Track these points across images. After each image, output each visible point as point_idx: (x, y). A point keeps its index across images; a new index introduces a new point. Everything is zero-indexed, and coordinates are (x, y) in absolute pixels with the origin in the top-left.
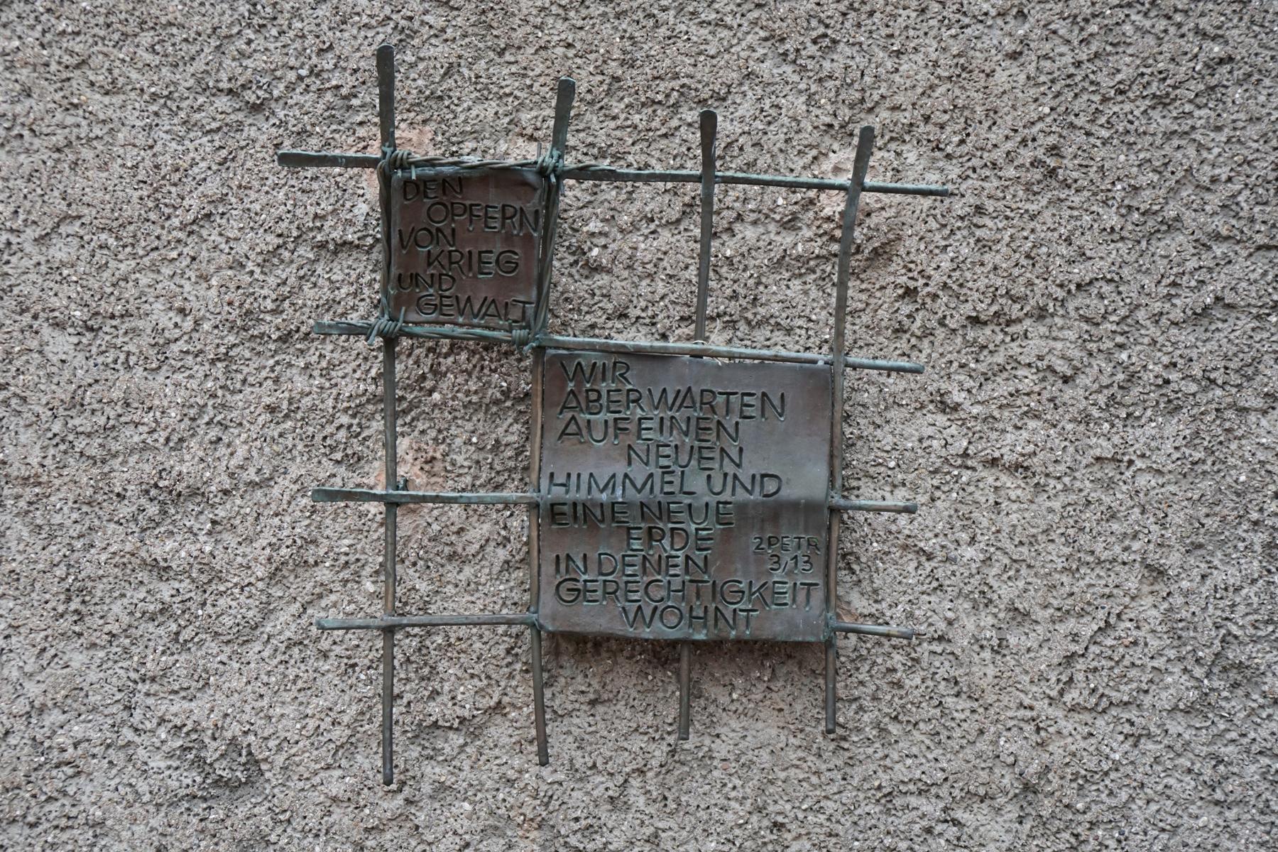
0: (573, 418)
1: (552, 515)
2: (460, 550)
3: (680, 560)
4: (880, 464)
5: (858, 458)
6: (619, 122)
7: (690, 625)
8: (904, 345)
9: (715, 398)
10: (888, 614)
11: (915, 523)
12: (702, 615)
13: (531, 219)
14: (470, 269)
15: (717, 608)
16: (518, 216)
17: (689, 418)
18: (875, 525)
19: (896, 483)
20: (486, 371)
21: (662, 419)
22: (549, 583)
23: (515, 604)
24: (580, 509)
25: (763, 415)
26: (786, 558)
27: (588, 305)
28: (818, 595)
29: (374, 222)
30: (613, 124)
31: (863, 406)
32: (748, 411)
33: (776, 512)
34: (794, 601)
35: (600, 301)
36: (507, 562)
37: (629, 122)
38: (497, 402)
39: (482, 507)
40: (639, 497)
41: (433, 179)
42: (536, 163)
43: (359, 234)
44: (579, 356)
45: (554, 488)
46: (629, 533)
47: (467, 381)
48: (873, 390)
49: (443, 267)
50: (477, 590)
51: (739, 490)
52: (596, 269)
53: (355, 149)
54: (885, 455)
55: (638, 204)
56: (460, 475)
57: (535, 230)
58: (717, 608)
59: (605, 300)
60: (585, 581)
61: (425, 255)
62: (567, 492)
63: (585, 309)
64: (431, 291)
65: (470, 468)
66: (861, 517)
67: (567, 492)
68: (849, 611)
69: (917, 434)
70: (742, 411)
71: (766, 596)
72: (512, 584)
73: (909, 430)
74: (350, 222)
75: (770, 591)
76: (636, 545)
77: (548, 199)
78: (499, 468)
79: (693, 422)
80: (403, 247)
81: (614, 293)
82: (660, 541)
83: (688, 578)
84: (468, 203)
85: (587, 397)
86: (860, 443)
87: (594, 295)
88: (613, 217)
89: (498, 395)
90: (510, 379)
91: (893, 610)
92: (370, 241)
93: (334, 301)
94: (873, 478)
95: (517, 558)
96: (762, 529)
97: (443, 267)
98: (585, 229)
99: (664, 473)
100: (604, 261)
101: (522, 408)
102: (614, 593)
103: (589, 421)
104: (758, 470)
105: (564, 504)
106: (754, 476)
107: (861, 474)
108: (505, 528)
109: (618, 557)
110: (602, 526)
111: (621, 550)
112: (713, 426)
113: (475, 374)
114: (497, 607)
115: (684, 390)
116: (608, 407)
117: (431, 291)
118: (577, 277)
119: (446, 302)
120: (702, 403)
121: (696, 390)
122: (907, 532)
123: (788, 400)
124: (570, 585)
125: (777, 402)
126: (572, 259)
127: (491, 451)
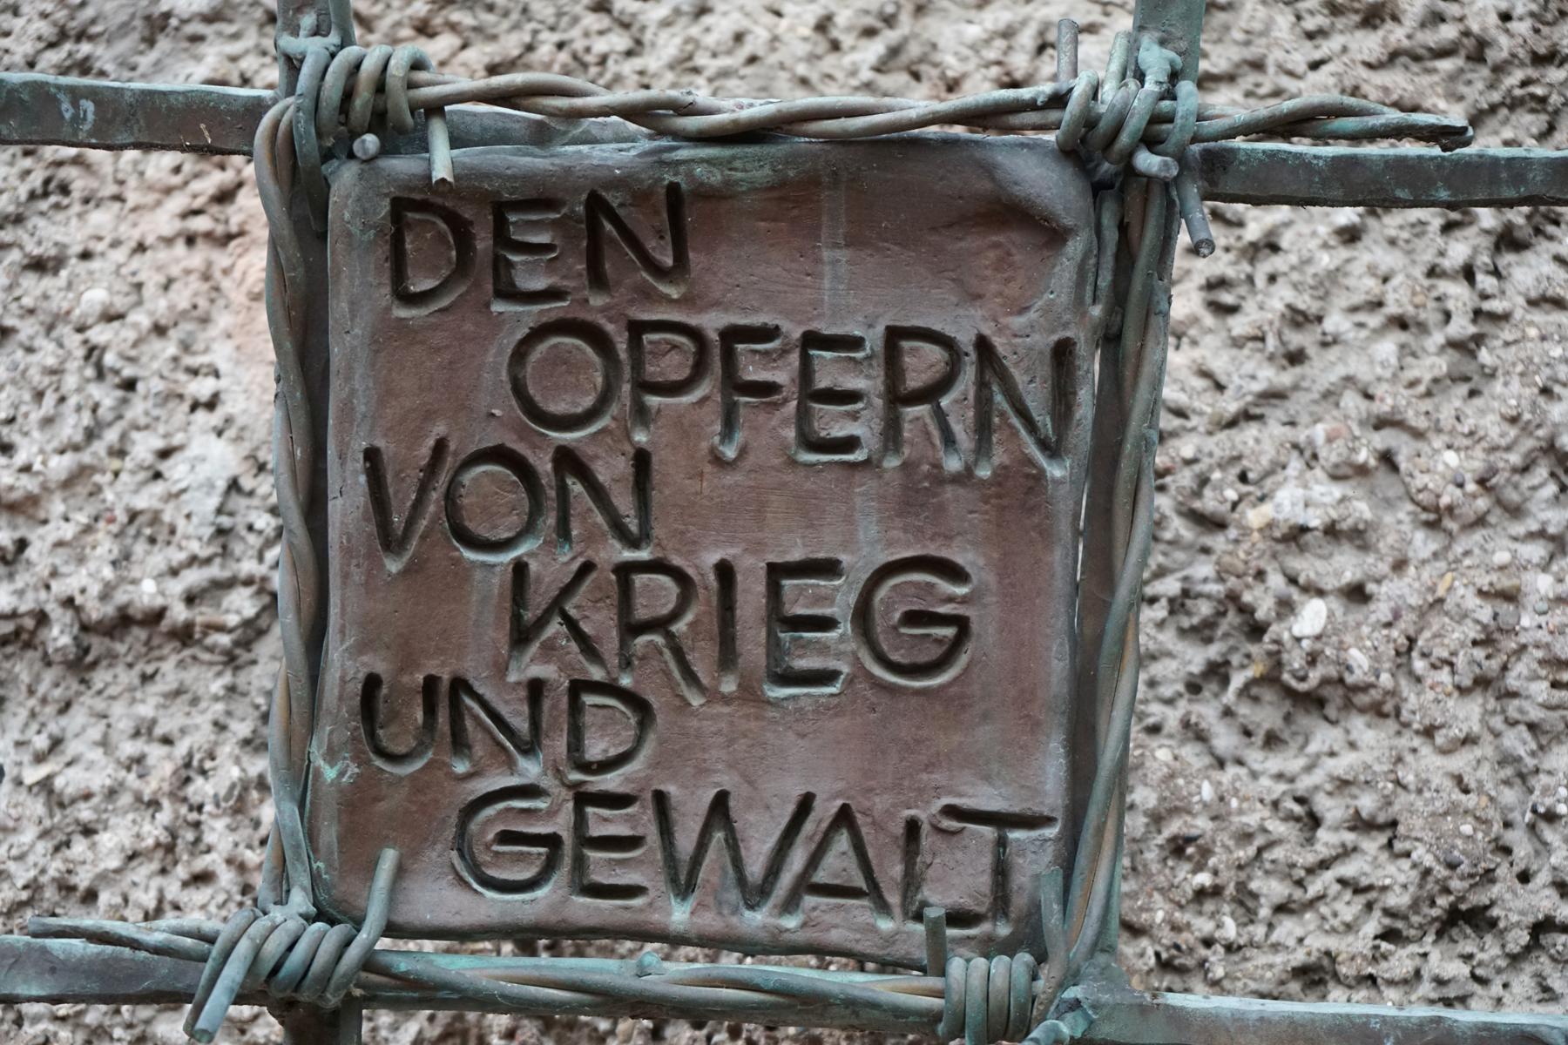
6: (1397, 35)
13: (1036, 396)
14: (727, 656)
16: (967, 381)
27: (1286, 871)
29: (264, 522)
30: (1369, 44)
35: (1346, 852)
37: (1448, 32)
41: (540, 198)
42: (1059, 100)
43: (194, 577)
49: (589, 647)
52: (1313, 702)
53: (178, 202)
55: (1510, 393)
57: (1053, 450)
59: (1372, 844)
61: (499, 582)
63: (1272, 889)
64: (530, 770)
74: (145, 527)
77: (1119, 299)
80: (390, 541)
81: (1414, 816)
84: (712, 322)
87: (1314, 821)
88: (1387, 459)
92: (241, 605)
93: (66, 888)
97: (589, 647)
98: (1255, 517)
100: (1359, 659)
117: (530, 770)
118: (1225, 739)
119: (602, 823)
126: (1196, 657)
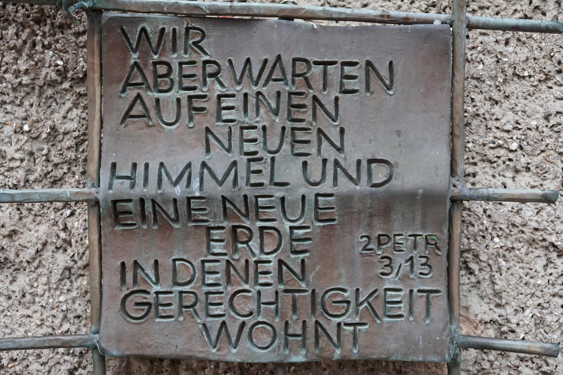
0: (139, 96)
1: (114, 214)
2: (12, 256)
3: (272, 266)
4: (500, 146)
5: (476, 138)
7: (286, 345)
8: (525, 7)
9: (309, 68)
10: (514, 320)
11: (543, 213)
12: (300, 332)
15: (317, 322)
17: (279, 93)
18: (495, 217)
19: (519, 167)
20: (39, 48)
21: (246, 95)
22: (113, 297)
23: (79, 317)
24: (148, 206)
25: (368, 89)
26: (400, 259)
28: (440, 303)
31: (478, 79)
32: (350, 84)
33: (387, 205)
34: (411, 312)
36: (69, 269)
38: (52, 84)
39: (37, 206)
40: (220, 191)
44: (143, 20)
45: (116, 182)
46: (208, 234)
47: (16, 59)
48: (489, 60)
50: (34, 303)
51: (342, 179)
54: (506, 135)
56: (10, 169)
58: (317, 322)
60: (157, 293)
62: (133, 186)
65: (22, 160)
66: (477, 207)
67: (133, 186)
68: (468, 319)
69: (542, 110)
70: (342, 84)
71: (376, 307)
72: (74, 294)
73: (532, 105)
75: (381, 301)
76: (218, 248)
78: (56, 160)
79: (284, 98)
82: (246, 242)
83: (282, 287)
85: (155, 71)
86: (475, 122)
89: (53, 75)
90: (66, 56)
91: (520, 316)
94: (491, 162)
95: (80, 263)
96: (370, 226)
99: (249, 160)
101: (81, 90)
102: (193, 306)
103: (158, 100)
104: (364, 155)
105: (130, 201)
106: (359, 162)
107: (478, 158)
108: (65, 229)
109: (197, 263)
110: (176, 226)
111: (200, 255)
112: (308, 102)
113: (26, 51)
114: (57, 322)
115: (272, 60)
116: (181, 83)
120: (294, 75)
121: (287, 60)
122: (534, 225)
123: (397, 69)
124: (139, 298)
125: (384, 73)
127: (47, 140)
